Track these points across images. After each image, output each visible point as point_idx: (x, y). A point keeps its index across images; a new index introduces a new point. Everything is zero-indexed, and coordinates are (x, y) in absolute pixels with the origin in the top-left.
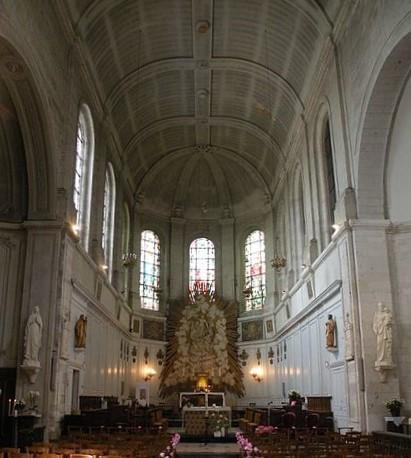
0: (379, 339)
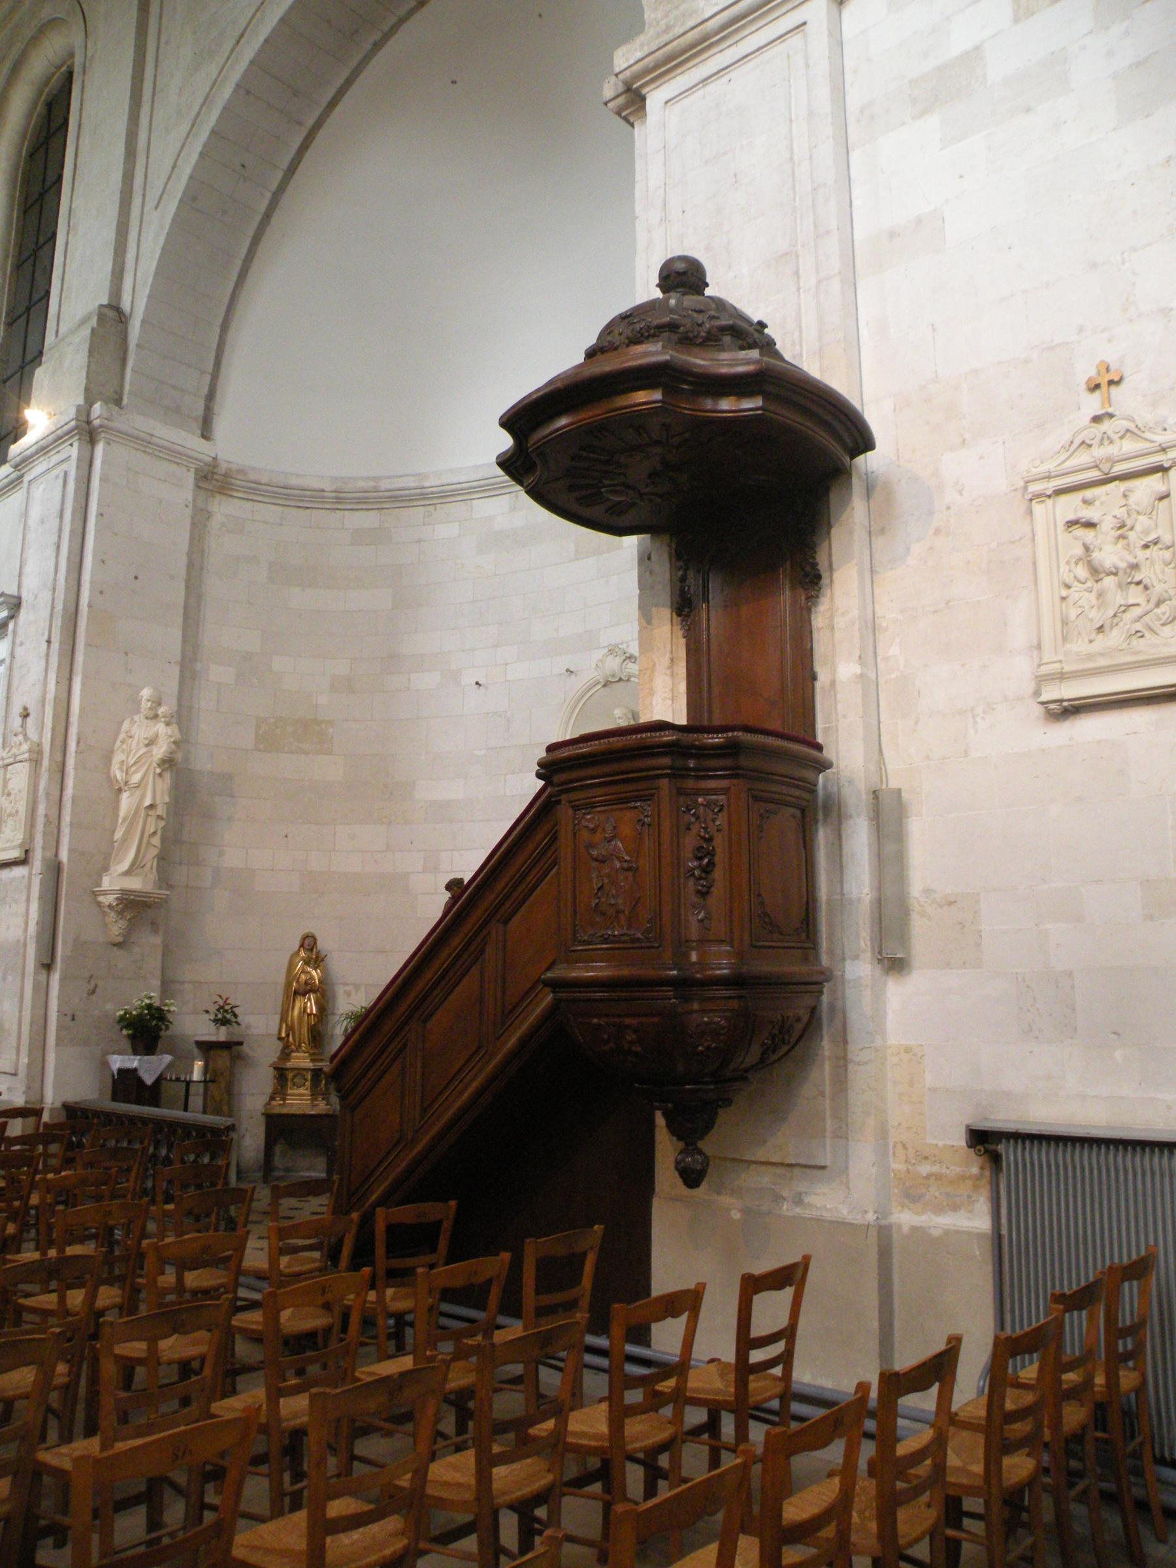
0: (126, 802)
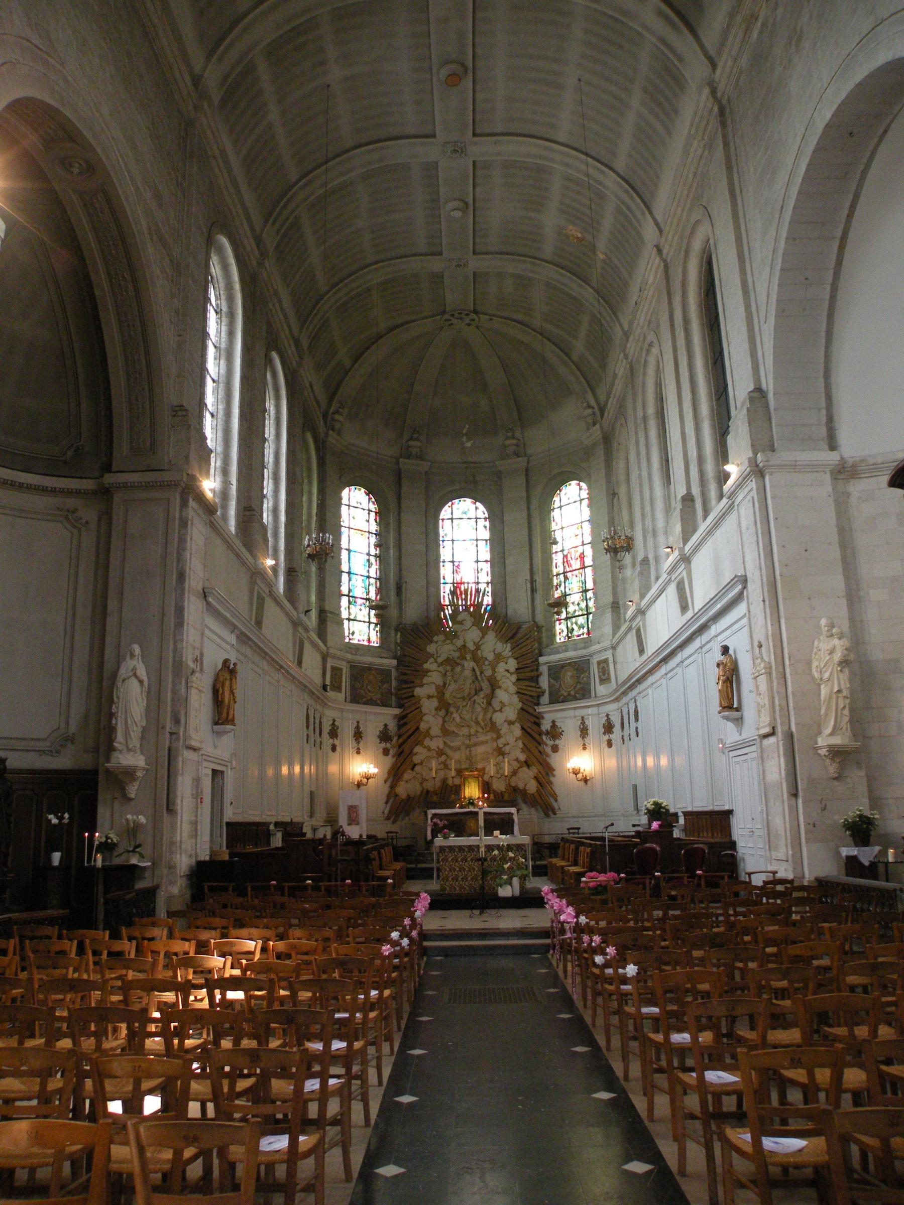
0: (824, 691)
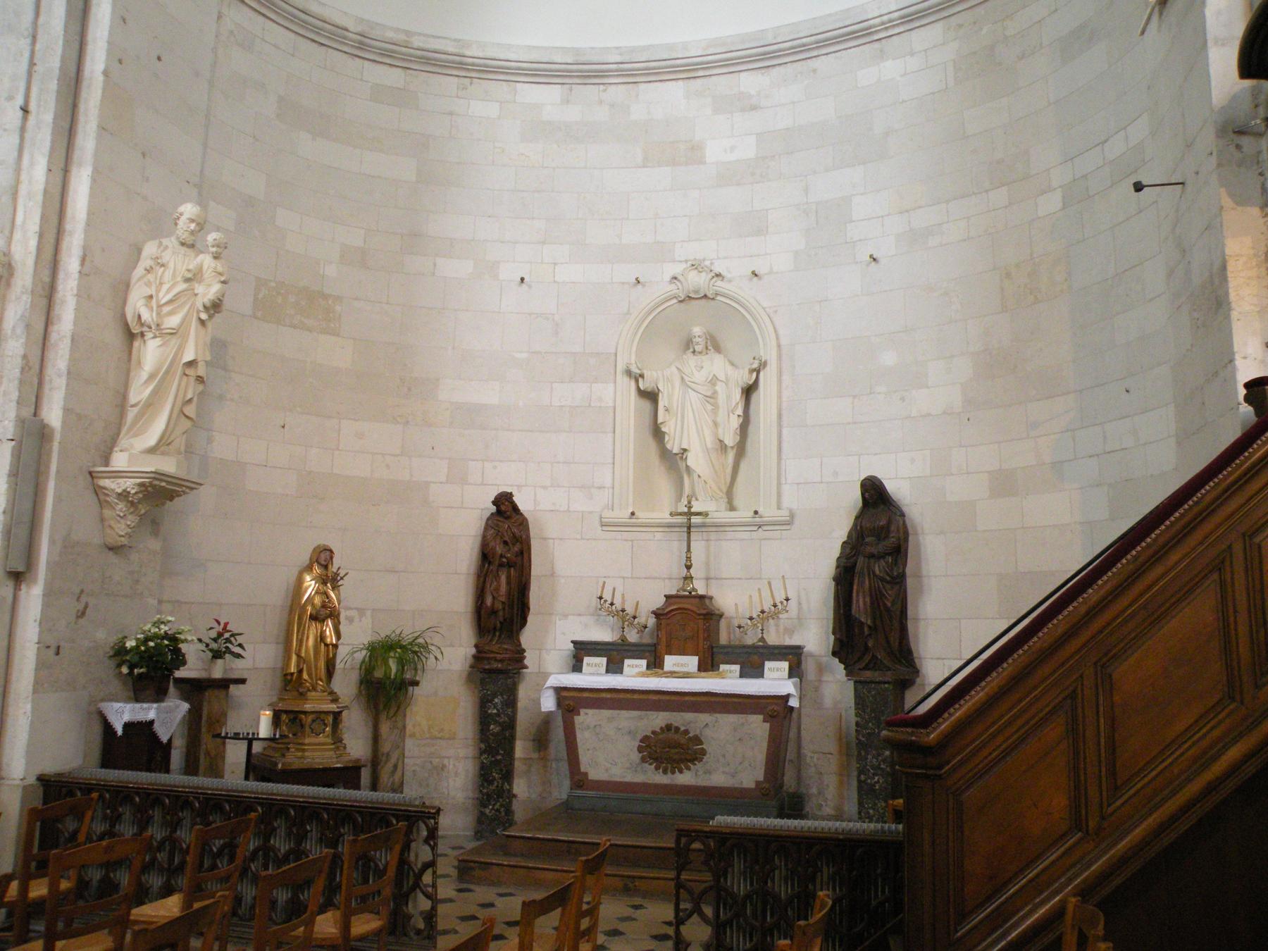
0: (151, 353)
